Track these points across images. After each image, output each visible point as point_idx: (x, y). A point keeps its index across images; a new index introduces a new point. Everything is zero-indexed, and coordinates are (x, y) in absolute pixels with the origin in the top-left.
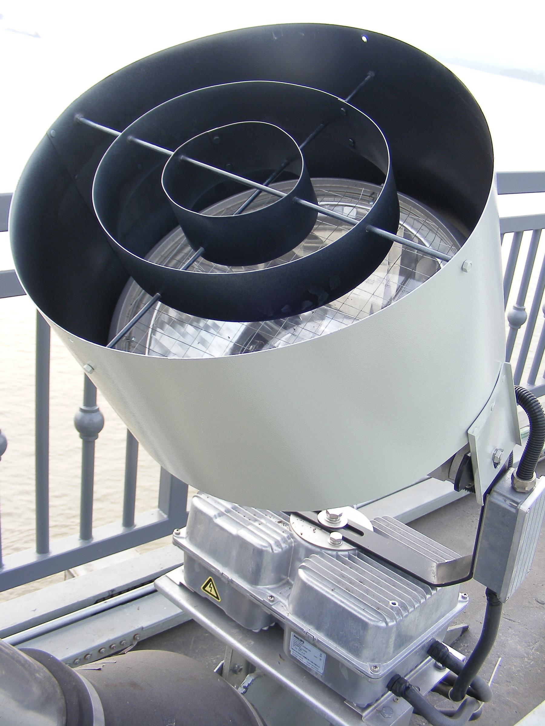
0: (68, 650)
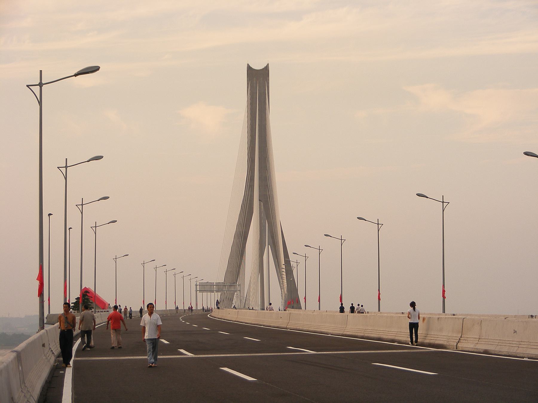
0: (513, 332)
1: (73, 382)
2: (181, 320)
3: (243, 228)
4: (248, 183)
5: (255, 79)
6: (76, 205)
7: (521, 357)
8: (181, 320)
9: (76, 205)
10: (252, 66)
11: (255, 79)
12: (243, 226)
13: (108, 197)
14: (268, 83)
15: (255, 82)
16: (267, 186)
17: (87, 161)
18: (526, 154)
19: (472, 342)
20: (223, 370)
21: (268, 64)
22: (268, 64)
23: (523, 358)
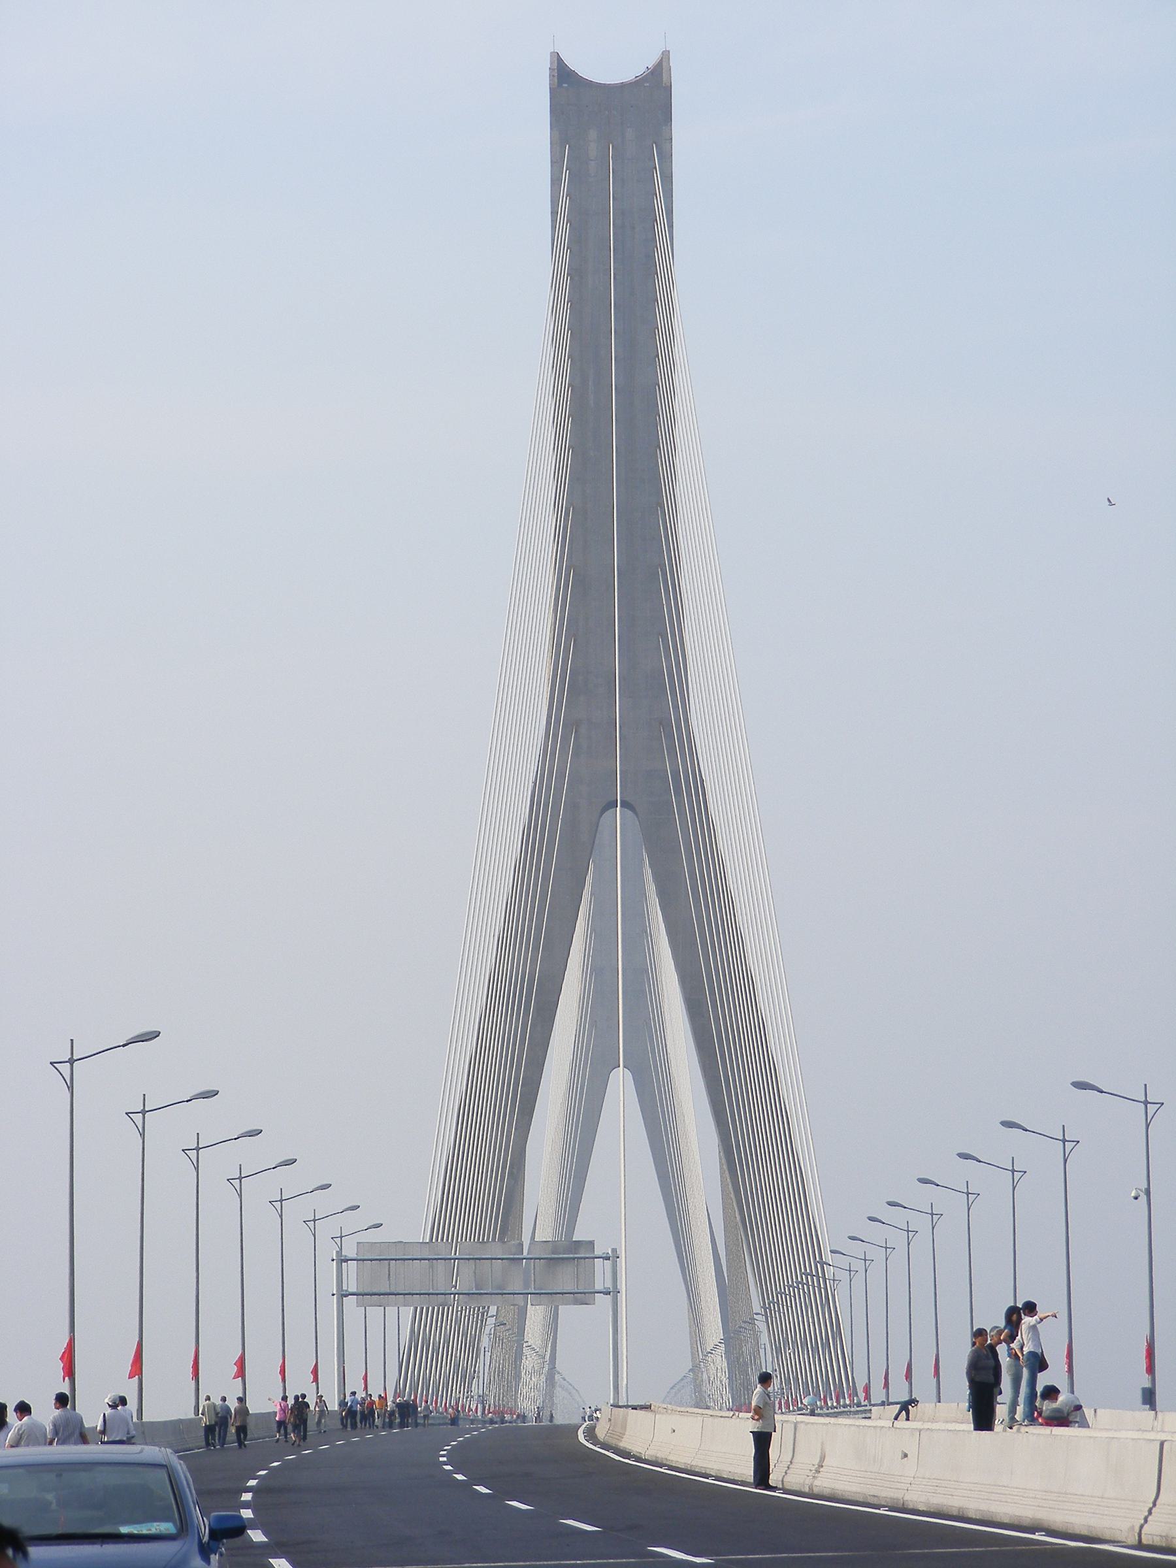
1: (1061, 1546)
2: (448, 1468)
3: (534, 961)
4: (559, 709)
5: (593, 134)
6: (183, 1150)
7: (869, 1503)
8: (448, 1468)
9: (183, 1150)
10: (573, 64)
11: (593, 134)
12: (536, 948)
13: (157, 1034)
14: (666, 157)
15: (593, 150)
16: (665, 723)
17: (69, 1095)
18: (850, 1238)
19: (960, 1485)
20: (272, 1466)
21: (666, 55)
22: (666, 55)
23: (1032, 1530)
